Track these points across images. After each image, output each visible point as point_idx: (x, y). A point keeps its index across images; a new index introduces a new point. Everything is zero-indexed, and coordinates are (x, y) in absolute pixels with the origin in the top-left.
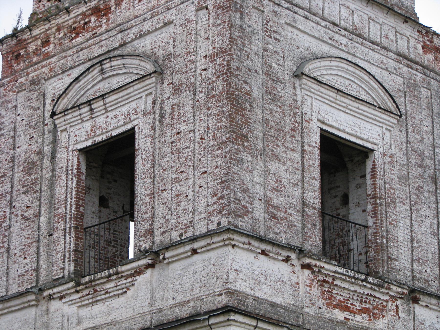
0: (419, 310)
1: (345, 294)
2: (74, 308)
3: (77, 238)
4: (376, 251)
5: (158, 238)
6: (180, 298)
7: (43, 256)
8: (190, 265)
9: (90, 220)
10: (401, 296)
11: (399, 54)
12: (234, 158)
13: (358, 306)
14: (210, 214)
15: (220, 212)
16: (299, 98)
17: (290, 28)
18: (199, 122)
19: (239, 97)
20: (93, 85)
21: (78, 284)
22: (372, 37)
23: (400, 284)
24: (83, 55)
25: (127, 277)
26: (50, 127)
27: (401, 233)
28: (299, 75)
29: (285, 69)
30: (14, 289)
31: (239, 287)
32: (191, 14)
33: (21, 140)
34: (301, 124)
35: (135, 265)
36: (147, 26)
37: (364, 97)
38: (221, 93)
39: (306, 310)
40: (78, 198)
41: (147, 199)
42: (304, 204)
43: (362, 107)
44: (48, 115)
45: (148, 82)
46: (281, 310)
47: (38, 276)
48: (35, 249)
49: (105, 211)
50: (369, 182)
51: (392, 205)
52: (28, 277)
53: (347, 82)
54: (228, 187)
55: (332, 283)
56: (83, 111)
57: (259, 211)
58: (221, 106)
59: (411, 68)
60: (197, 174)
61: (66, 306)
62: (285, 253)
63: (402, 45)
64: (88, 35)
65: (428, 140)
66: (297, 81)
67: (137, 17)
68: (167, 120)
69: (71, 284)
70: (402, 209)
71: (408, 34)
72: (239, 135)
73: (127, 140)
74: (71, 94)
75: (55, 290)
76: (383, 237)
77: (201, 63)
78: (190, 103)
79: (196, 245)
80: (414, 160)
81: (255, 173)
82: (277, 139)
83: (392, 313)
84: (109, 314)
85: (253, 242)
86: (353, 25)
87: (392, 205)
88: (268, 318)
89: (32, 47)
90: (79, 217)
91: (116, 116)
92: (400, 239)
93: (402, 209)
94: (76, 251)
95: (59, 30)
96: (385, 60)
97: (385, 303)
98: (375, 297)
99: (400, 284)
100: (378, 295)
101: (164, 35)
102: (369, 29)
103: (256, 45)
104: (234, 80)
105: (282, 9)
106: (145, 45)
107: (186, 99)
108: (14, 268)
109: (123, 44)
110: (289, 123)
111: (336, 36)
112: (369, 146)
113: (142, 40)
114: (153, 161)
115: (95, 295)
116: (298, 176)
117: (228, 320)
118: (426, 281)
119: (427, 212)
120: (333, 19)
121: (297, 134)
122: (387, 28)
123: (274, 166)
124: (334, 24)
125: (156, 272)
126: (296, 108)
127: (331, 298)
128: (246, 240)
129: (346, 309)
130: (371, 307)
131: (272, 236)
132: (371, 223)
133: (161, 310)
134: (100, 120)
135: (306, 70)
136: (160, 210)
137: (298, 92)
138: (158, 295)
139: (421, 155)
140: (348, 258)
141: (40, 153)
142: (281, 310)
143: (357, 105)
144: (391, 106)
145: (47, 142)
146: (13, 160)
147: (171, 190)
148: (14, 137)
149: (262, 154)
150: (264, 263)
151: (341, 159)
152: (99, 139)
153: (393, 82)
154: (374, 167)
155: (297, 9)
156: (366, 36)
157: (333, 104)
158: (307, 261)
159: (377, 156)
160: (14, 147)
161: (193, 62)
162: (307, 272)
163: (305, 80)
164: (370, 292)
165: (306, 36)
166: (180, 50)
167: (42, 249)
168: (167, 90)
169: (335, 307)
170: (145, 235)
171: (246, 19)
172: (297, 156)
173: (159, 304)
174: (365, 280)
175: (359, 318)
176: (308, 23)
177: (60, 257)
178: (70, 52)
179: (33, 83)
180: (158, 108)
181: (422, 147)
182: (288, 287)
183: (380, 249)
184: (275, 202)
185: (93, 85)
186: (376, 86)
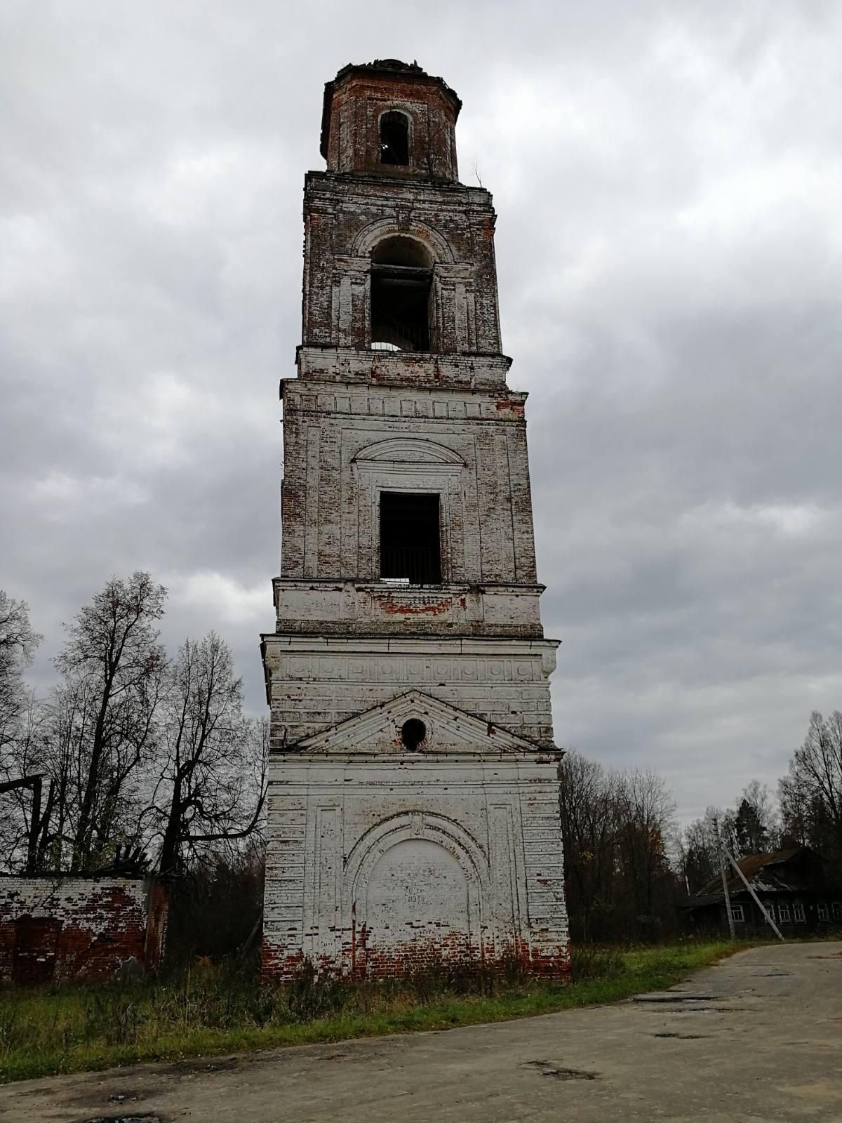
13: (422, 607)
31: (288, 617)
37: (429, 459)
43: (419, 467)
46: (330, 625)
48: (261, 814)
53: (409, 453)
55: (389, 597)
59: (482, 424)
63: (473, 411)
76: (448, 553)
82: (331, 509)
83: (456, 606)
85: (299, 584)
88: (366, 634)
97: (449, 600)
98: (436, 597)
100: (439, 596)
102: (434, 409)
105: (338, 420)
110: (345, 494)
111: (396, 424)
123: (327, 528)
128: (293, 584)
130: (436, 605)
131: (324, 575)
142: (330, 625)
143: (416, 466)
144: (457, 459)
153: (455, 441)
155: (353, 416)
156: (431, 415)
157: (394, 472)
162: (361, 593)
163: (359, 463)
164: (430, 595)
165: (366, 432)
169: (396, 612)
174: (422, 588)
175: (422, 615)
186: (438, 448)
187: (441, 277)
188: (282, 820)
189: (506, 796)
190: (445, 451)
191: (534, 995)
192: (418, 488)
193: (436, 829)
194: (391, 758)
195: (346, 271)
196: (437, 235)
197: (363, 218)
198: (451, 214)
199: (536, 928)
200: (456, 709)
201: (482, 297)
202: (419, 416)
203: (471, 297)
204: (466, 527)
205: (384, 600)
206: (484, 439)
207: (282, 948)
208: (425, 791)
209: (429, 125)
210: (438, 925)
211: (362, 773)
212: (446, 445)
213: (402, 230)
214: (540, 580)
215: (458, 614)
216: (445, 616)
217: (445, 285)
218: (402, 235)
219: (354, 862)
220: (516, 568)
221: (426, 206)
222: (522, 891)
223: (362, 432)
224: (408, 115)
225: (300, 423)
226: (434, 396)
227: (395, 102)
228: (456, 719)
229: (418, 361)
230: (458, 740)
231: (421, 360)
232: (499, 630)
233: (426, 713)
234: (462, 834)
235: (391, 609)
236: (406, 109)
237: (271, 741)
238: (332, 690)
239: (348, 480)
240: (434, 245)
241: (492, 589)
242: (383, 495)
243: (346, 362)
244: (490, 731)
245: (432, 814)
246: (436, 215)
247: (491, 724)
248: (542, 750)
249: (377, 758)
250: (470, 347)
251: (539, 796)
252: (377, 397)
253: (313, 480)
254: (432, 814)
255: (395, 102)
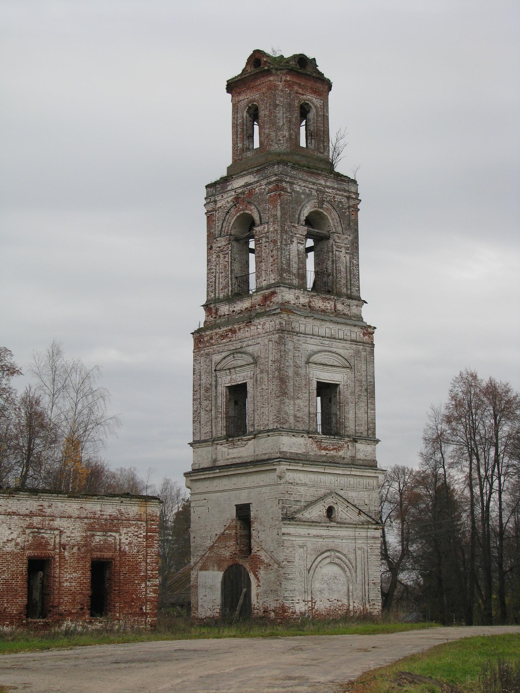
0: (357, 445)
1: (326, 444)
2: (226, 449)
3: (226, 421)
4: (340, 425)
5: (256, 428)
6: (264, 452)
7: (214, 427)
8: (268, 440)
9: (232, 413)
10: (350, 441)
11: (352, 341)
12: (282, 402)
14: (274, 422)
15: (277, 422)
16: (308, 372)
17: (304, 344)
18: (270, 386)
19: (284, 378)
20: (230, 362)
21: (228, 441)
22: (340, 337)
23: (349, 436)
24: (226, 348)
25: (245, 441)
26: (214, 374)
27: (351, 416)
28: (308, 362)
29: (301, 362)
30: (203, 438)
31: (284, 450)
32: (267, 343)
33: (203, 377)
34: (309, 382)
35: (248, 437)
36: (250, 343)
38: (277, 377)
39: (310, 453)
40: (226, 406)
41: (252, 412)
42: (310, 414)
44: (213, 369)
45: (251, 366)
47: (212, 434)
49: (237, 407)
50: (338, 397)
51: (347, 405)
52: (208, 434)
54: (280, 414)
56: (227, 371)
57: (292, 420)
58: (276, 382)
60: (269, 406)
61: (223, 448)
62: (302, 435)
63: (354, 336)
64: (228, 340)
65: (364, 374)
66: (307, 365)
67: (246, 338)
68: (258, 383)
69: (225, 440)
70: (352, 405)
71: (356, 330)
72: (283, 393)
73: (244, 386)
74: (222, 363)
75: (219, 442)
77: (270, 363)
78: (267, 378)
79: (269, 434)
80: (357, 384)
81: (290, 406)
84: (239, 453)
86: (331, 334)
87: (347, 405)
89: (206, 339)
90: (227, 413)
91: (240, 376)
92: (350, 418)
93: (352, 405)
94: (226, 427)
95: (216, 334)
96: (345, 345)
99: (349, 436)
101: (257, 348)
103: (291, 354)
104: (282, 372)
106: (250, 349)
107: (265, 375)
108: (202, 430)
109: (242, 347)
110: (304, 382)
111: (324, 342)
112: (338, 383)
113: (249, 347)
114: (254, 397)
115: (234, 446)
116: (308, 403)
117: (336, 312)
118: (361, 433)
119: (363, 404)
120: (322, 335)
121: (307, 386)
122: (346, 331)
123: (298, 402)
124: (323, 337)
125: (256, 440)
126: (307, 376)
127: (321, 446)
128: (286, 433)
129: (327, 449)
131: (297, 428)
132: (338, 413)
133: (257, 455)
134: (234, 377)
135: (311, 360)
136: (257, 417)
137: (308, 369)
138: (256, 449)
139: (361, 381)
140: (331, 424)
141: (211, 385)
145: (213, 380)
146: (200, 385)
147: (260, 410)
148: (200, 376)
149: (293, 398)
150: (294, 439)
151: (326, 390)
152: (233, 384)
154: (340, 391)
155: (307, 336)
156: (337, 337)
158: (310, 435)
159: (341, 386)
160: (200, 380)
161: (268, 362)
162: (310, 439)
163: (310, 364)
166: (262, 356)
167: (213, 424)
168: (258, 371)
169: (322, 449)
170: (251, 426)
171: (286, 347)
172: (307, 395)
173: (257, 452)
174: (334, 438)
175: (332, 452)
176: (312, 340)
177: (220, 429)
178: (221, 345)
179: (207, 354)
180: (255, 376)
181: (361, 378)
182: (303, 446)
183: (342, 424)
184: (298, 415)
185: (230, 362)
187: (336, 242)
188: (287, 551)
189: (362, 545)
190: (343, 360)
191: (144, 636)
192: (327, 380)
193: (339, 558)
194: (325, 525)
195: (296, 234)
196: (335, 213)
197: (303, 196)
198: (340, 197)
199: (371, 603)
200: (348, 502)
201: (353, 258)
202: (332, 338)
203: (348, 257)
204: (350, 404)
205: (318, 443)
206: (357, 353)
207: (289, 608)
208: (335, 540)
209: (324, 118)
210: (338, 600)
211: (314, 531)
212: (343, 356)
213: (319, 207)
214: (377, 437)
215: (346, 453)
216: (341, 453)
217: (337, 248)
218: (319, 210)
219: (311, 572)
220: (368, 429)
221: (330, 191)
222: (367, 587)
223: (310, 345)
224: (313, 107)
225: (286, 338)
226: (339, 327)
227: (308, 97)
228: (347, 507)
229: (328, 300)
230: (347, 517)
231: (330, 299)
232: (361, 462)
233: (336, 504)
234: (347, 561)
235: (320, 448)
236: (313, 103)
237: (282, 514)
238: (302, 489)
239: (304, 374)
240: (333, 219)
241: (360, 441)
242: (318, 383)
243: (298, 298)
244: (359, 514)
245: (338, 552)
246: (334, 197)
247: (360, 510)
248: (377, 523)
249: (321, 524)
250: (347, 291)
251: (374, 545)
252: (316, 324)
253: (291, 373)
254: (338, 552)
255: (308, 97)
